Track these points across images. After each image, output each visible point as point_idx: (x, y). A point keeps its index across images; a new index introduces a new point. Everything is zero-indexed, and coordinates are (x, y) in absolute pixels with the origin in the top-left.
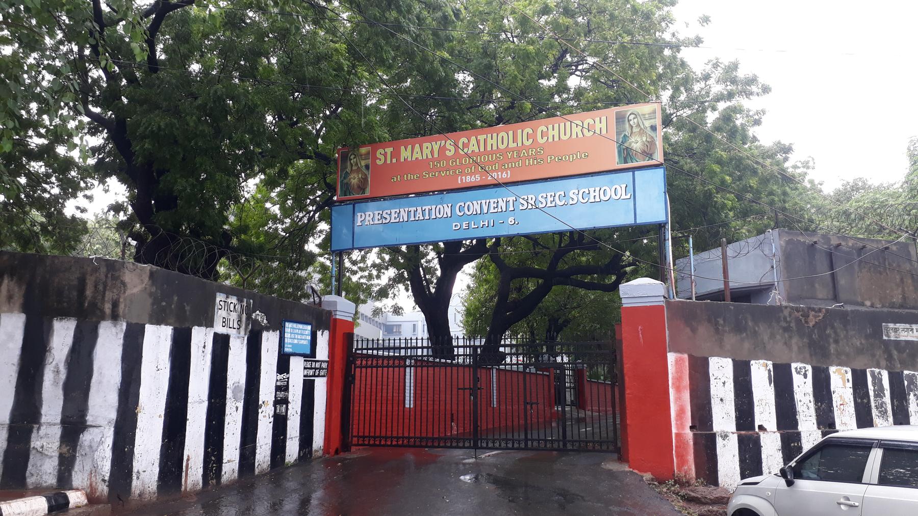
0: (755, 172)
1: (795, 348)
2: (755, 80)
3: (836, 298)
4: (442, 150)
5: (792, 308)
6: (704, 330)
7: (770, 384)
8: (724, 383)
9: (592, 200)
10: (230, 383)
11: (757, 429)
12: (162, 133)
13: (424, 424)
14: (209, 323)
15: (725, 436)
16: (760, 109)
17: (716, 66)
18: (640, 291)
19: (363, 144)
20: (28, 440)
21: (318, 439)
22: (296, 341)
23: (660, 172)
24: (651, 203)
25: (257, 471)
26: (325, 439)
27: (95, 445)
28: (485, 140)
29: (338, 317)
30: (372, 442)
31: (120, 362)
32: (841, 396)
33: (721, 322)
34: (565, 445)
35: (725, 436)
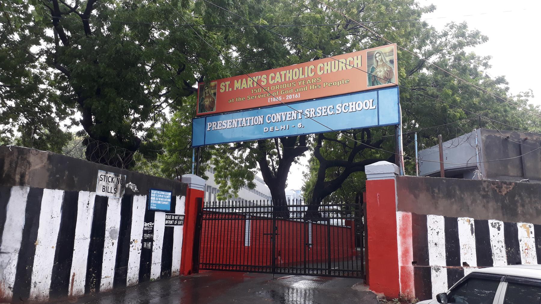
0: (478, 95)
1: (491, 210)
2: (401, 4)
3: (523, 176)
5: (489, 182)
6: (423, 197)
7: (472, 234)
8: (438, 233)
9: (351, 110)
10: (108, 227)
11: (462, 265)
12: (83, 74)
14: (93, 189)
15: (437, 269)
16: (486, 55)
17: (452, 27)
18: (380, 170)
19: (213, 80)
21: (176, 264)
22: (159, 202)
23: (395, 90)
24: (388, 110)
25: (128, 284)
27: (4, 265)
28: (285, 74)
29: (192, 188)
30: (211, 268)
32: (526, 244)
33: (436, 191)
34: (330, 273)
35: (437, 269)
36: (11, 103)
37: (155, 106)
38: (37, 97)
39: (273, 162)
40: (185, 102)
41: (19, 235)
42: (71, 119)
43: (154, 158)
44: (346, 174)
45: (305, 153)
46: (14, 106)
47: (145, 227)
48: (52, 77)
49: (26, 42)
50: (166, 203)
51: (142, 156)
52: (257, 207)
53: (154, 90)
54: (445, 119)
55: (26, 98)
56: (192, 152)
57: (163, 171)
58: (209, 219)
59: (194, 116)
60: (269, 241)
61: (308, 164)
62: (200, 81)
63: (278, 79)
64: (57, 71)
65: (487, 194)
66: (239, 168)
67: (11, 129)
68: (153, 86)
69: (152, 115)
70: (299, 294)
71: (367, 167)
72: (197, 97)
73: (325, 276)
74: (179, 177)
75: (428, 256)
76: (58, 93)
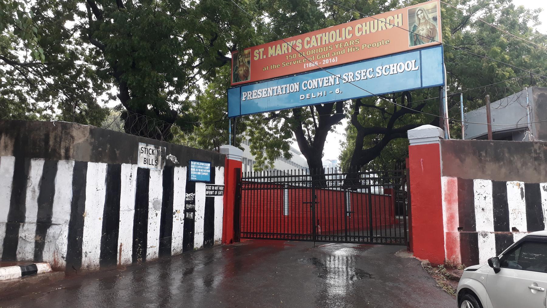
0: (529, 51)
4: (293, 48)
5: (541, 143)
6: (469, 160)
7: (522, 198)
8: (485, 198)
9: (392, 73)
11: (511, 230)
12: (118, 50)
13: (297, 226)
15: (485, 235)
16: (537, 8)
18: (423, 134)
20: (17, 233)
22: (199, 173)
23: (439, 49)
24: (431, 71)
25: (173, 253)
26: (223, 234)
27: (56, 236)
28: (321, 38)
29: (230, 158)
31: (71, 185)
33: (484, 154)
34: (372, 240)
35: (485, 235)
36: (50, 80)
37: (189, 78)
38: (74, 73)
39: (309, 132)
40: (218, 72)
41: (68, 208)
42: (107, 93)
43: (191, 131)
44: (386, 141)
45: (342, 121)
46: (53, 83)
47: (186, 197)
48: (87, 53)
49: (60, 18)
50: (206, 174)
51: (179, 129)
52: (288, 177)
53: (187, 62)
54: (492, 80)
55: (63, 75)
56: (227, 122)
57: (200, 143)
58: (248, 189)
59: (228, 86)
60: (309, 210)
61: (345, 132)
62: (233, 50)
63: (314, 43)
64: (92, 46)
65: (539, 156)
66: (274, 139)
67: (51, 106)
68: (186, 57)
69: (186, 87)
70: (341, 262)
71: (410, 132)
72: (231, 66)
73: (367, 243)
74: (217, 148)
75: (475, 221)
76: (94, 68)
